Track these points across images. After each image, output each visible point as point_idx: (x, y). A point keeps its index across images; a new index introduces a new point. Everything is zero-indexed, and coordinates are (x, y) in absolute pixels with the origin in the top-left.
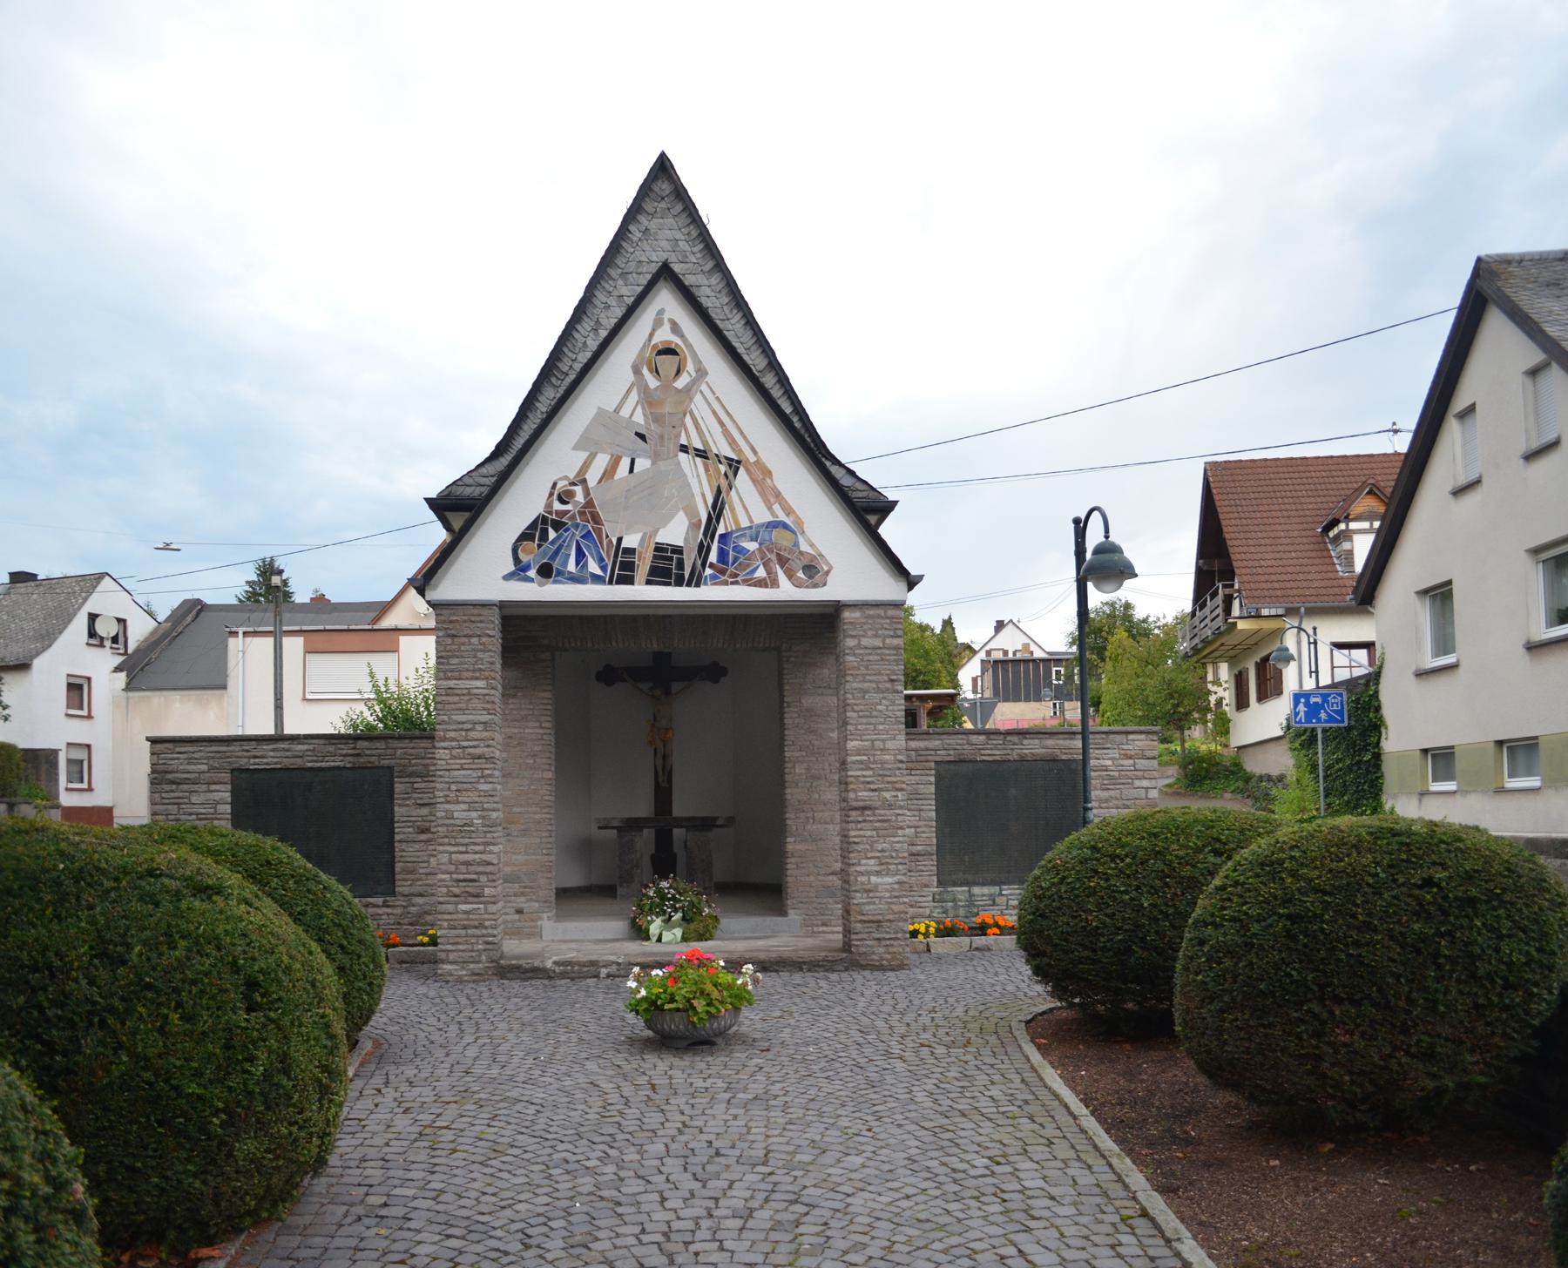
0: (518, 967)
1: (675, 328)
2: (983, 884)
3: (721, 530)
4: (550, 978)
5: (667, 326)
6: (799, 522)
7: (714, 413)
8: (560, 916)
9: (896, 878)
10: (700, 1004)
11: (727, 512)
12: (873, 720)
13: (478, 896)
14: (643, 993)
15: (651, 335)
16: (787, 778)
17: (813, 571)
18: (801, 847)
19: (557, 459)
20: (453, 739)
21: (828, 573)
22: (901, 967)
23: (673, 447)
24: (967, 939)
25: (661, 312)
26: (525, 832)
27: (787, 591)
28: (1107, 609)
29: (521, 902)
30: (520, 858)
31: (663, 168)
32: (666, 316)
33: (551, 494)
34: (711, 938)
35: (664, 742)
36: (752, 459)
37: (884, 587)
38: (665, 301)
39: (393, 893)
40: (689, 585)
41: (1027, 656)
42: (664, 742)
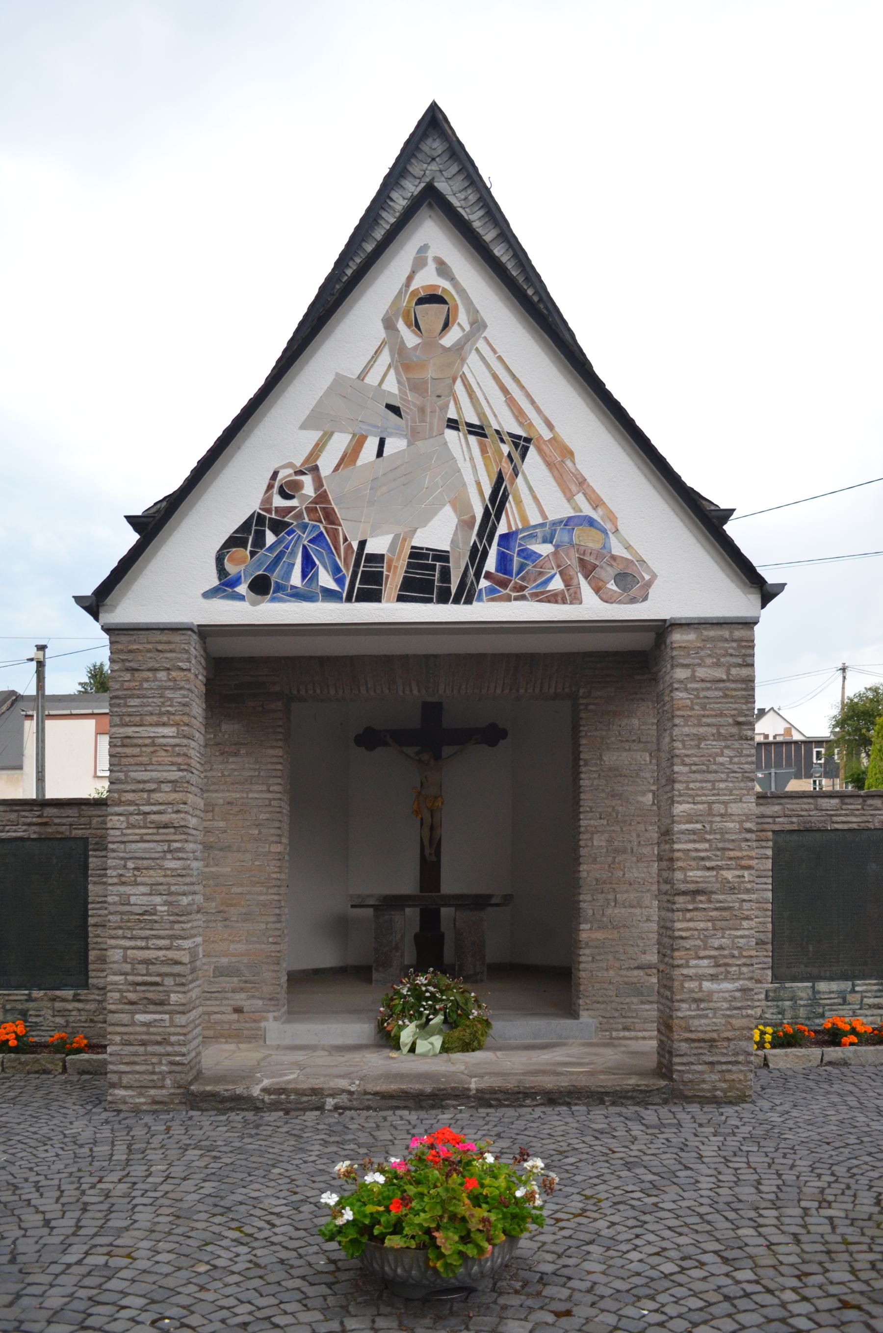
0: (214, 1095)
1: (443, 269)
2: (832, 979)
3: (502, 528)
4: (257, 1109)
5: (431, 266)
6: (611, 517)
7: (495, 377)
8: (294, 1013)
9: (737, 984)
10: (448, 1241)
11: (510, 505)
12: (711, 777)
13: (161, 1003)
14: (348, 1215)
15: (410, 279)
16: (583, 852)
17: (631, 581)
18: (599, 935)
19: (281, 443)
20: (131, 803)
21: (649, 584)
22: (742, 1099)
23: (437, 422)
24: (816, 1052)
25: (424, 249)
26: (247, 917)
27: (590, 607)
28: (870, 695)
29: (240, 999)
30: (240, 947)
31: (434, 122)
32: (430, 255)
33: (270, 487)
34: (480, 1048)
35: (432, 812)
36: (547, 435)
37: (726, 599)
38: (430, 236)
39: (86, 985)
40: (457, 601)
41: (788, 738)
42: (432, 812)
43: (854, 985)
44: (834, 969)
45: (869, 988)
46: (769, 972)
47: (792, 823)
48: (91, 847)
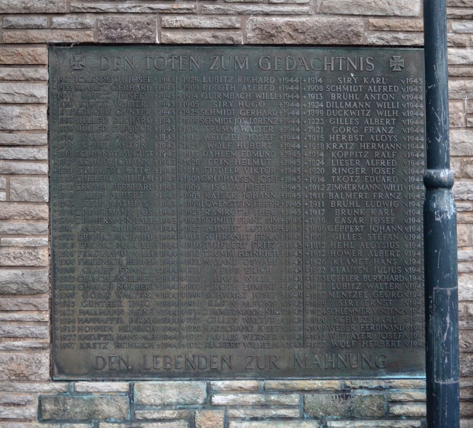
2: (169, 375)
43: (210, 391)
44: (172, 352)
45: (240, 398)
46: (45, 358)
47: (85, 27)
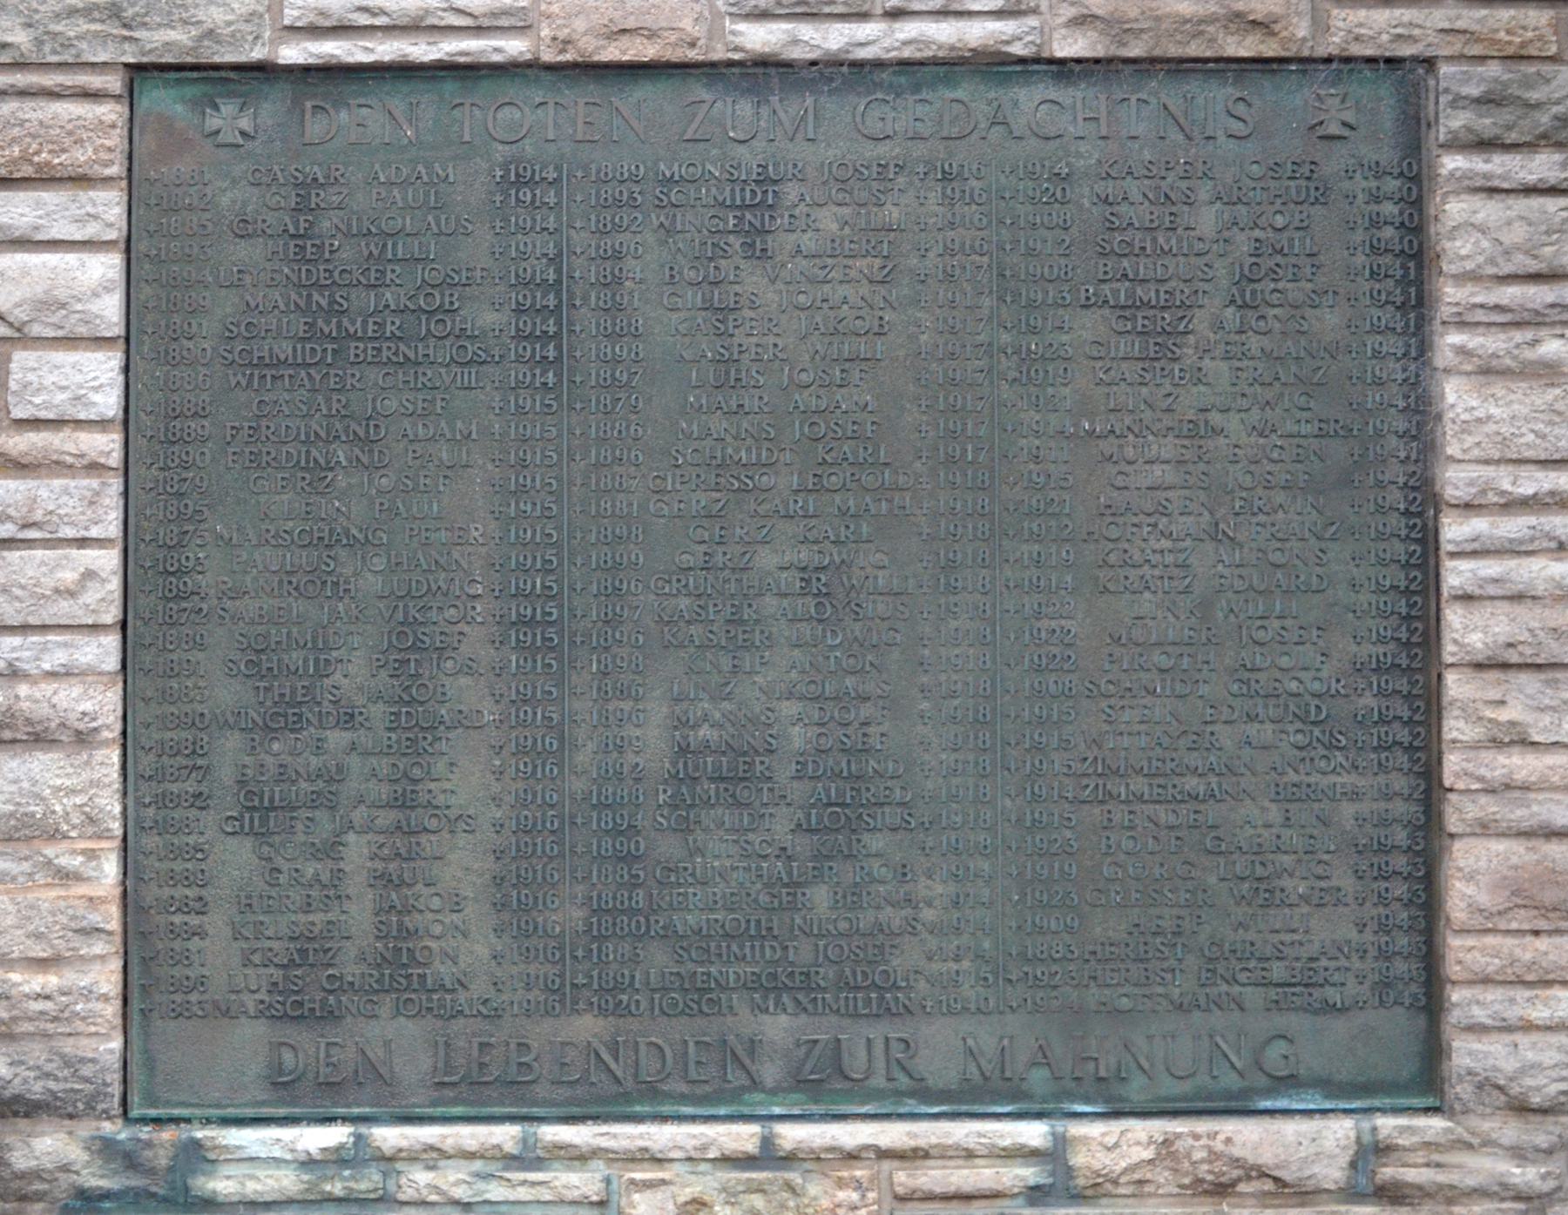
39: (1425, 1079)
48: (1455, 121)
